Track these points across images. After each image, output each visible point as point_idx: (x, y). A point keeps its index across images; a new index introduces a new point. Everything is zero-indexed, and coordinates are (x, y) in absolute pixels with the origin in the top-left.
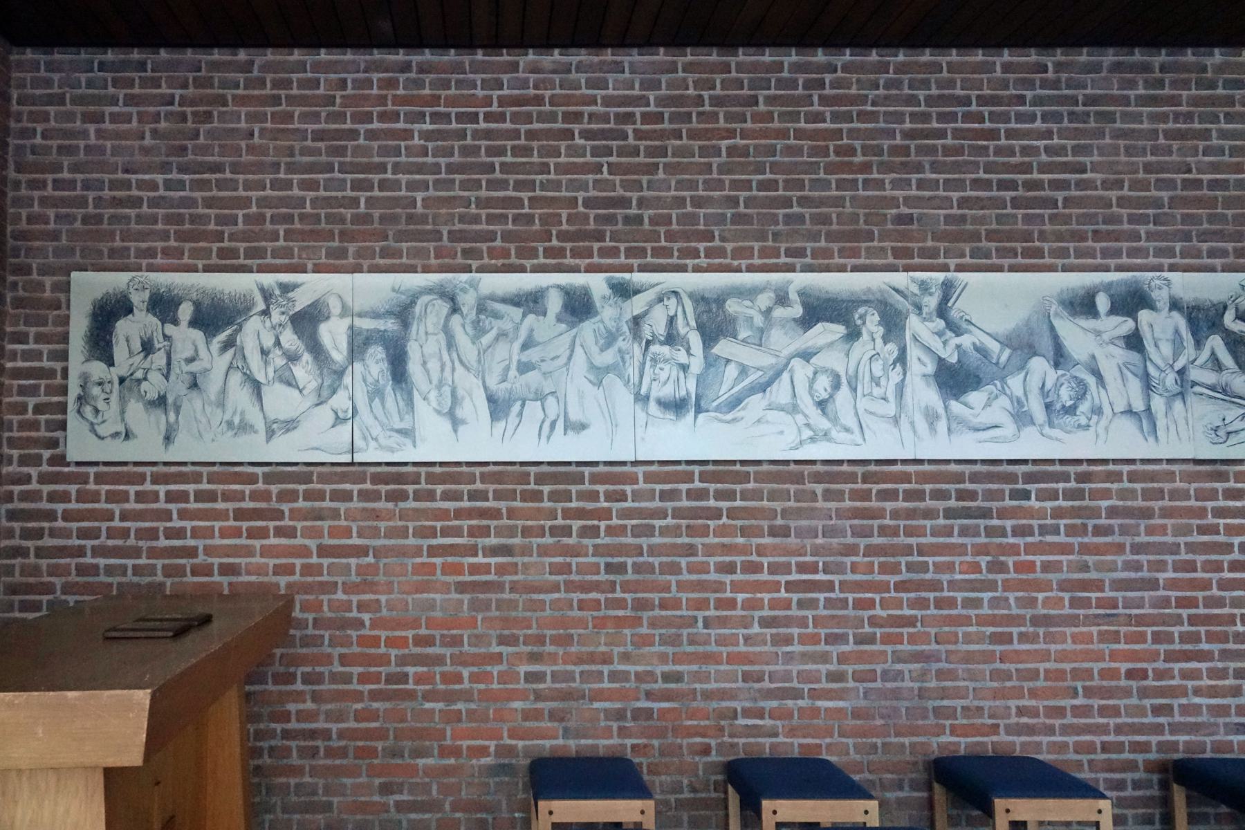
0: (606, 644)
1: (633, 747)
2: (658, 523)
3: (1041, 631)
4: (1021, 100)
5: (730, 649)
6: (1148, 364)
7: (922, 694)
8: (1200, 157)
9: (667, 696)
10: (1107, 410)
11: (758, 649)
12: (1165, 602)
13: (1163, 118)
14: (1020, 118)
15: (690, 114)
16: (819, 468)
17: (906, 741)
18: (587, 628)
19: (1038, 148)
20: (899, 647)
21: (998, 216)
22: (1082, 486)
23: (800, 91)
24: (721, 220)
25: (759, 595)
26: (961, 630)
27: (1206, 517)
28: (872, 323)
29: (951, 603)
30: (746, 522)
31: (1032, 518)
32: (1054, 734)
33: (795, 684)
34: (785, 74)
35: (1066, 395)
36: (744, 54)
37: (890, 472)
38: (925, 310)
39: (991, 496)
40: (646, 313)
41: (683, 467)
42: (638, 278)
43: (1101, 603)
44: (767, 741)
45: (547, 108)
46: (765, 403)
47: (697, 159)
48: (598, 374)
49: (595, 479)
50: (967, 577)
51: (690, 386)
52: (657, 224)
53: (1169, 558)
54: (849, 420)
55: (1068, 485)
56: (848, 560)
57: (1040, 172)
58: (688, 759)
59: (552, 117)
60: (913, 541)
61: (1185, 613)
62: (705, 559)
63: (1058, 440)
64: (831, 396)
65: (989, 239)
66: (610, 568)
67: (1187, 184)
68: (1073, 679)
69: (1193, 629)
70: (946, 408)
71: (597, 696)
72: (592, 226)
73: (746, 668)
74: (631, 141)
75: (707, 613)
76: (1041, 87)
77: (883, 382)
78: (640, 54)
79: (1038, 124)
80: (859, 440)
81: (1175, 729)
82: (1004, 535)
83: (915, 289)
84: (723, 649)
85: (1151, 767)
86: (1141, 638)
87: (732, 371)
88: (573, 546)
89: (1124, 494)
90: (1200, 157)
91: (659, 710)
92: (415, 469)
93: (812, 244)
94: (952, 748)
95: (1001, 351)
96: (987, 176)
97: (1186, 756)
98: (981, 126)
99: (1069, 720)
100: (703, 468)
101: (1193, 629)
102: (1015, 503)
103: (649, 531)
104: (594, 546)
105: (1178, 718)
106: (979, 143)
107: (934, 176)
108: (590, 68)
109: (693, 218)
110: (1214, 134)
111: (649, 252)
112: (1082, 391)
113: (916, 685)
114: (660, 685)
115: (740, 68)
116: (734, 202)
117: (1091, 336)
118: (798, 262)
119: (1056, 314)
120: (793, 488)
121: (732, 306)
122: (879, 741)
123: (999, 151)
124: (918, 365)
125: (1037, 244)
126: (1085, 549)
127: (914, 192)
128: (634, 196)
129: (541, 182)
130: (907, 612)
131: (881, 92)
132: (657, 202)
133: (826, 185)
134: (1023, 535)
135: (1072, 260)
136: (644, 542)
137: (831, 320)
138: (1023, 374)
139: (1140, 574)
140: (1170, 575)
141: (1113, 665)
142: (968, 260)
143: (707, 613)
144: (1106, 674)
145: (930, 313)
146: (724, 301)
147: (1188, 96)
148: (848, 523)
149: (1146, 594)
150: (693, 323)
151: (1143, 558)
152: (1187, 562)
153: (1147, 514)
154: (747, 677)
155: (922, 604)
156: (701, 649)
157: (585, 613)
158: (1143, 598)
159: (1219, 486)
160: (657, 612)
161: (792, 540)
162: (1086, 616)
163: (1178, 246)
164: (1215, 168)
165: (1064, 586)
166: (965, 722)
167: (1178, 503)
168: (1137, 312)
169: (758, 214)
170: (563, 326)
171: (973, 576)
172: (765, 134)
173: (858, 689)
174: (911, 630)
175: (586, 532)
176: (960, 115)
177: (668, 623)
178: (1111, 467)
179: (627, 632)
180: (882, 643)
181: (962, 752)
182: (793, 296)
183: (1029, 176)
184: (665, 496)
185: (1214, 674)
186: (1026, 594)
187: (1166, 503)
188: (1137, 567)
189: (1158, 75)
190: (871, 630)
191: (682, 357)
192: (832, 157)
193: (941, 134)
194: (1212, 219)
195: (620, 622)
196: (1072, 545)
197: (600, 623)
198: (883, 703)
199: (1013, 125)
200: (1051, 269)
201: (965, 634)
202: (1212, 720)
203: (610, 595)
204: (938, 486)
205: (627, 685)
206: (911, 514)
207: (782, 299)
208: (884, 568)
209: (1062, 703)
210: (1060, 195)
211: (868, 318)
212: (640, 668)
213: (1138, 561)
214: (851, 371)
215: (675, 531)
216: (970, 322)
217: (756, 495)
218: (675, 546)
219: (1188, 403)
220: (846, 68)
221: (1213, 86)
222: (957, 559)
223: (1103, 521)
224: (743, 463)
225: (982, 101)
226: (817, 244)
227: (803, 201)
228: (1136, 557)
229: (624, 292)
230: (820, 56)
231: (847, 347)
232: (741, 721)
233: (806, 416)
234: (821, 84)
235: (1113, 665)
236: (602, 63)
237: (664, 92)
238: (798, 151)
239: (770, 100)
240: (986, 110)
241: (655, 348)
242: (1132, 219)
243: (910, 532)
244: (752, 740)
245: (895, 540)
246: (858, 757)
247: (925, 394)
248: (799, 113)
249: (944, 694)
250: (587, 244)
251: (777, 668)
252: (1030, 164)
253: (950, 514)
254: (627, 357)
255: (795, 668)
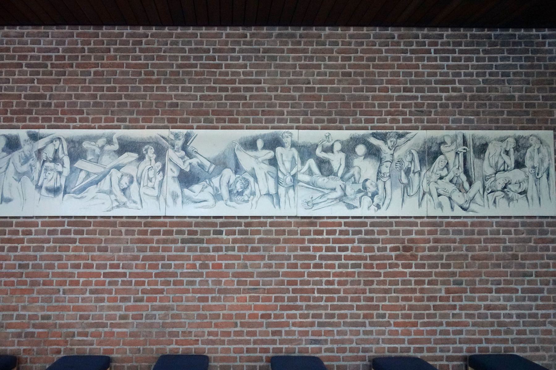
0: (16, 302)
1: (24, 350)
2: (46, 245)
3: (222, 296)
4: (233, 50)
5: (74, 304)
6: (279, 172)
7: (164, 325)
8: (315, 77)
9: (42, 326)
10: (258, 193)
11: (88, 304)
12: (282, 283)
13: (299, 59)
14: (232, 58)
15: (78, 56)
16: (124, 220)
17: (154, 347)
18: (7, 294)
19: (240, 72)
20: (154, 303)
21: (218, 104)
22: (248, 228)
23: (131, 46)
24: (87, 105)
25: (90, 279)
26: (184, 296)
27: (304, 243)
28: (151, 153)
29: (181, 283)
30: (88, 245)
31: (222, 243)
32: (224, 344)
33: (104, 321)
34: (124, 38)
35: (239, 187)
36: (106, 29)
37: (27, 222)
38: (176, 147)
39: (204, 233)
40: (44, 147)
41: (60, 219)
42: (42, 131)
43: (252, 283)
44: (88, 347)
45: (11, 53)
46: (98, 189)
47: (79, 77)
48: (19, 176)
49: (18, 225)
50: (189, 271)
51: (62, 182)
52: (58, 107)
53: (286, 262)
54: (136, 198)
55: (240, 228)
56: (134, 263)
57: (240, 83)
58: (50, 356)
59: (13, 58)
60: (166, 254)
61: (291, 288)
62: (66, 262)
63: (234, 207)
64: (128, 186)
65: (213, 114)
66: (21, 266)
67: (308, 89)
68: (236, 318)
69: (294, 295)
70: (182, 192)
71: (10, 326)
72: (27, 107)
73: (81, 313)
74: (49, 68)
75: (65, 287)
76: (244, 45)
77: (153, 180)
78: (57, 29)
79: (241, 61)
80: (140, 207)
81: (282, 342)
82: (209, 251)
83: (172, 137)
84: (71, 304)
85: (465, 359)
86: (269, 299)
87: (83, 175)
88: (5, 256)
89: (267, 232)
90: (315, 77)
91: (38, 333)
92: (441, 220)
93: (130, 116)
94: (176, 351)
95: (211, 166)
96: (214, 85)
97: (286, 355)
98: (214, 62)
99: (233, 337)
100: (69, 220)
101: (294, 295)
102: (215, 236)
103: (41, 249)
104: (15, 256)
105: (284, 337)
106: (212, 70)
107: (190, 85)
108: (33, 35)
109: (75, 104)
110: (322, 66)
111: (53, 120)
112: (247, 184)
113: (161, 321)
114: (40, 321)
115: (103, 35)
116: (95, 96)
117: (253, 159)
118: (122, 124)
119: (238, 149)
120: (111, 229)
121: (85, 145)
122: (141, 348)
123: (221, 74)
124: (172, 172)
125: (235, 116)
126: (246, 258)
127: (180, 93)
128: (48, 94)
129: (5, 87)
130: (160, 287)
131: (169, 46)
132: (58, 97)
133: (138, 89)
134: (218, 251)
135: (251, 124)
136: (38, 254)
137: (132, 151)
138: (220, 176)
139: (271, 270)
140: (285, 270)
141: (256, 312)
142: (202, 124)
143: (65, 287)
144: (251, 316)
145: (178, 148)
146: (82, 143)
147: (312, 49)
148: (135, 245)
149: (273, 279)
150: (66, 153)
151: (273, 262)
152: (293, 264)
153: (277, 241)
154: (81, 317)
155: (168, 283)
156: (61, 304)
157: (7, 287)
158: (272, 281)
159: (312, 228)
160: (41, 287)
161: (109, 254)
162: (244, 289)
163: (301, 118)
164: (321, 82)
165: (235, 275)
166: (182, 338)
167: (292, 237)
168: (276, 147)
169: (105, 102)
170: (5, 154)
171: (192, 270)
172: (113, 65)
173: (134, 323)
174: (161, 295)
175: (11, 249)
176: (204, 57)
177: (46, 292)
178: (262, 220)
179: (26, 296)
180: (147, 301)
181: (180, 353)
182: (115, 140)
183: (234, 85)
184: (50, 233)
185: (302, 316)
186: (217, 279)
187: (286, 236)
188: (270, 266)
189: (298, 39)
190: (142, 295)
191: (59, 168)
192: (143, 76)
193: (195, 66)
194: (318, 105)
195: (23, 292)
196: (240, 256)
197: (13, 292)
198: (145, 329)
199: (229, 62)
200: (241, 128)
201: (186, 297)
202: (300, 338)
203: (19, 279)
204: (179, 228)
205: (24, 321)
206: (165, 241)
207: (110, 142)
208: (151, 267)
209: (229, 330)
210: (248, 94)
211: (149, 151)
212: (30, 313)
213: (271, 264)
214: (139, 175)
215: (54, 249)
216: (197, 152)
217: (94, 232)
218: (53, 256)
219: (296, 191)
220: (152, 36)
221: (324, 44)
222: (185, 263)
223: (256, 245)
224: (89, 217)
225: (215, 51)
226: (132, 116)
227: (127, 96)
228: (270, 262)
229: (35, 138)
230: (141, 30)
231: (138, 164)
232: (77, 338)
233: (116, 196)
234: (140, 43)
235: (256, 312)
236: (39, 33)
237: (66, 46)
238: (127, 73)
239: (116, 50)
240: (216, 55)
241: (47, 164)
242: (281, 105)
243: (164, 250)
244: (80, 347)
245: (157, 254)
246: (131, 355)
247: (173, 186)
248: (129, 56)
249: (174, 325)
250: (24, 116)
251: (96, 313)
252: (235, 80)
253: (184, 241)
254: (33, 168)
255: (105, 313)
